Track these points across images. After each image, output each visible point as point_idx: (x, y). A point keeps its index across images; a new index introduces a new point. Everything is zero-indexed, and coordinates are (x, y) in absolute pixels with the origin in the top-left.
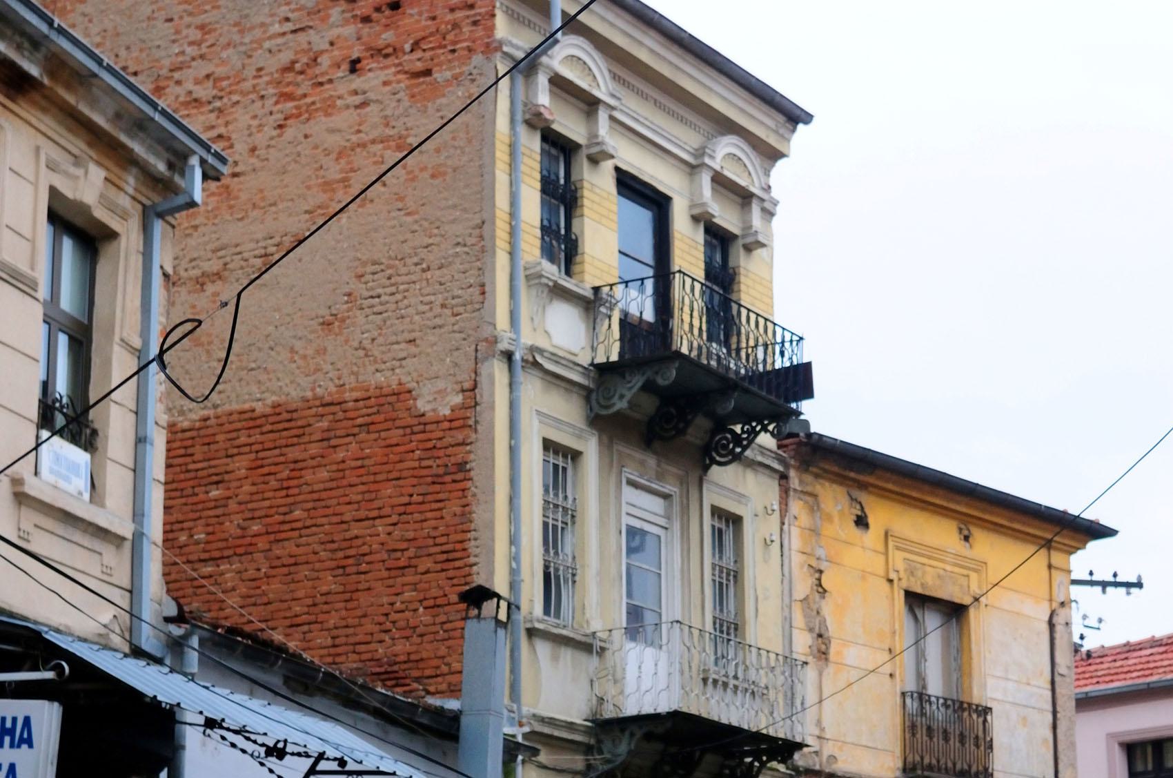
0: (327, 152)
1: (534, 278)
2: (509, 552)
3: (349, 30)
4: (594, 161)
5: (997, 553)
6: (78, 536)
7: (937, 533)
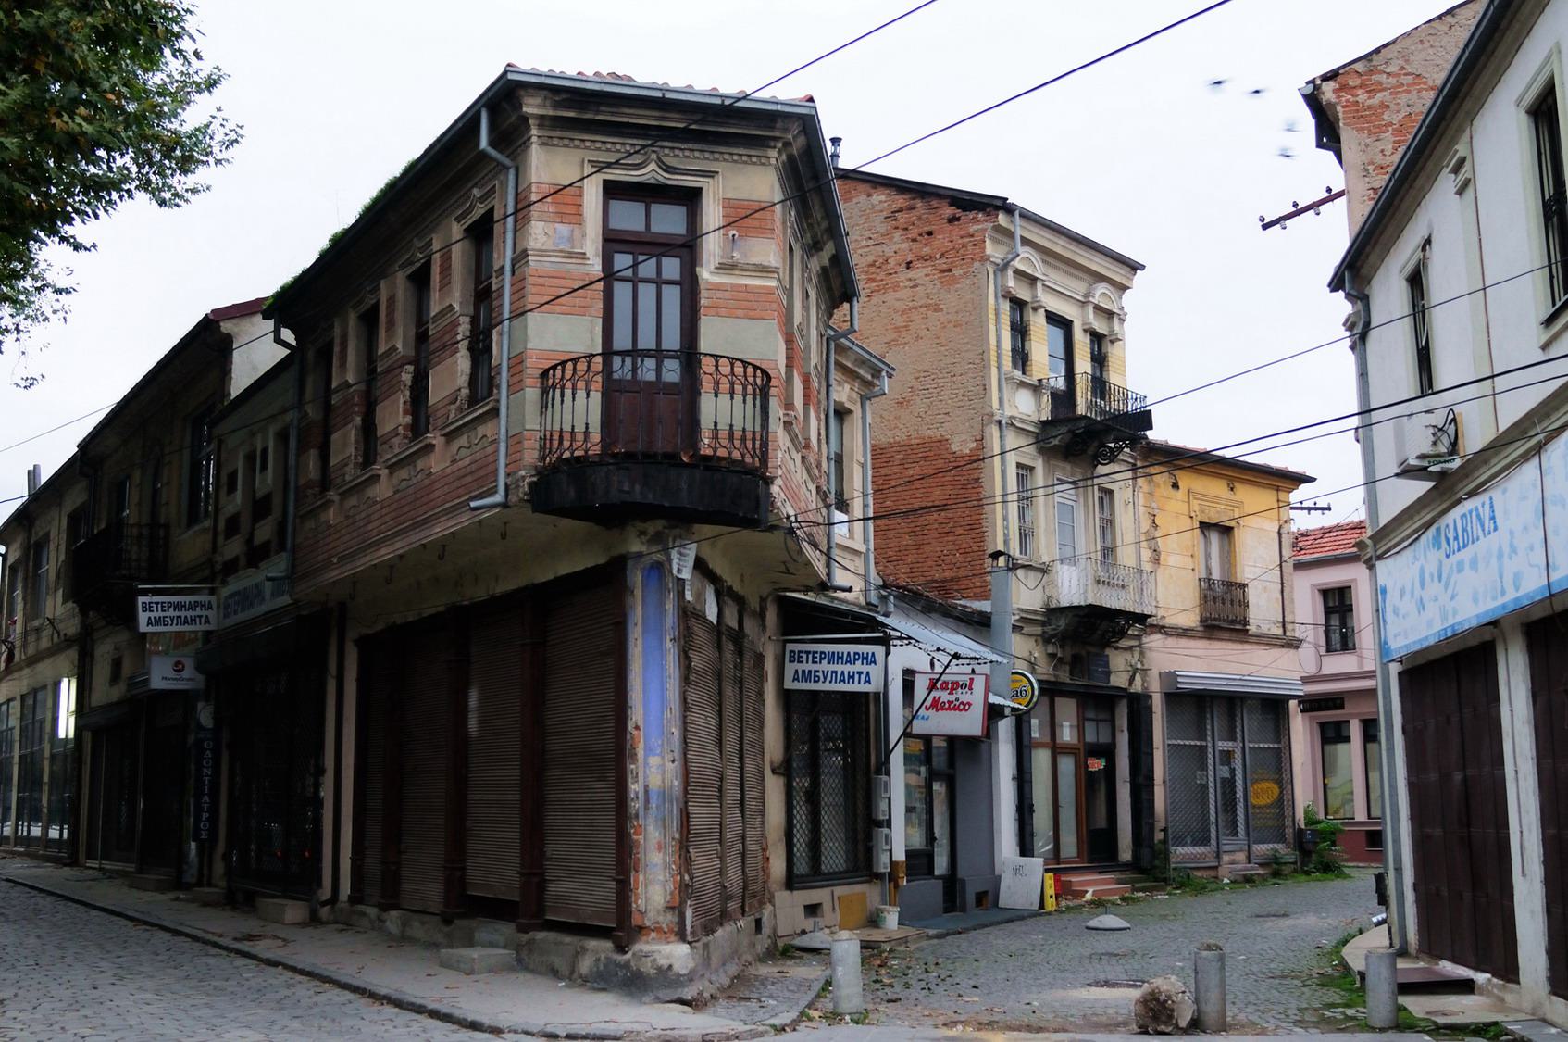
0: (896, 311)
1: (1010, 379)
2: (1002, 528)
3: (905, 246)
4: (1035, 309)
5: (1253, 498)
7: (1216, 488)
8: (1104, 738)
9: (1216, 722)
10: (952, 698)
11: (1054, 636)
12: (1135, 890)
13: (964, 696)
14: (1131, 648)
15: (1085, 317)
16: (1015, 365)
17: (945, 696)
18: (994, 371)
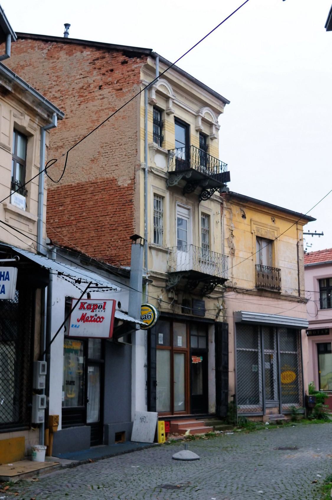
1: (151, 147)
2: (144, 226)
3: (99, 77)
4: (168, 114)
5: (282, 225)
6: (22, 221)
7: (265, 220)
8: (202, 346)
9: (263, 339)
10: (93, 314)
11: (173, 288)
12: (214, 429)
13: (100, 313)
14: (217, 299)
15: (197, 123)
16: (155, 140)
17: (89, 313)
18: (142, 142)
